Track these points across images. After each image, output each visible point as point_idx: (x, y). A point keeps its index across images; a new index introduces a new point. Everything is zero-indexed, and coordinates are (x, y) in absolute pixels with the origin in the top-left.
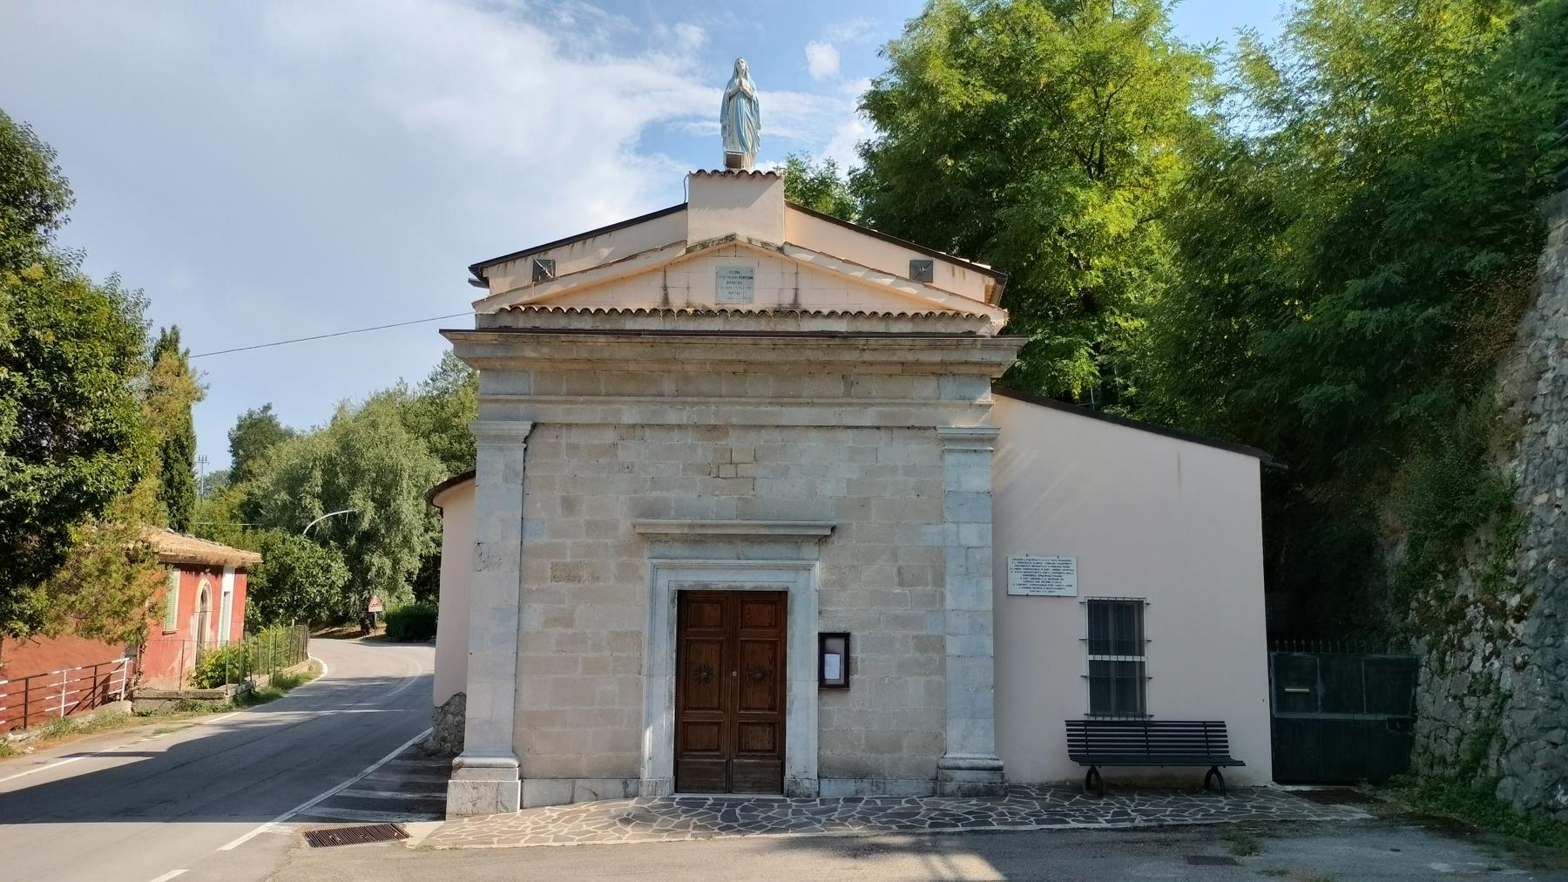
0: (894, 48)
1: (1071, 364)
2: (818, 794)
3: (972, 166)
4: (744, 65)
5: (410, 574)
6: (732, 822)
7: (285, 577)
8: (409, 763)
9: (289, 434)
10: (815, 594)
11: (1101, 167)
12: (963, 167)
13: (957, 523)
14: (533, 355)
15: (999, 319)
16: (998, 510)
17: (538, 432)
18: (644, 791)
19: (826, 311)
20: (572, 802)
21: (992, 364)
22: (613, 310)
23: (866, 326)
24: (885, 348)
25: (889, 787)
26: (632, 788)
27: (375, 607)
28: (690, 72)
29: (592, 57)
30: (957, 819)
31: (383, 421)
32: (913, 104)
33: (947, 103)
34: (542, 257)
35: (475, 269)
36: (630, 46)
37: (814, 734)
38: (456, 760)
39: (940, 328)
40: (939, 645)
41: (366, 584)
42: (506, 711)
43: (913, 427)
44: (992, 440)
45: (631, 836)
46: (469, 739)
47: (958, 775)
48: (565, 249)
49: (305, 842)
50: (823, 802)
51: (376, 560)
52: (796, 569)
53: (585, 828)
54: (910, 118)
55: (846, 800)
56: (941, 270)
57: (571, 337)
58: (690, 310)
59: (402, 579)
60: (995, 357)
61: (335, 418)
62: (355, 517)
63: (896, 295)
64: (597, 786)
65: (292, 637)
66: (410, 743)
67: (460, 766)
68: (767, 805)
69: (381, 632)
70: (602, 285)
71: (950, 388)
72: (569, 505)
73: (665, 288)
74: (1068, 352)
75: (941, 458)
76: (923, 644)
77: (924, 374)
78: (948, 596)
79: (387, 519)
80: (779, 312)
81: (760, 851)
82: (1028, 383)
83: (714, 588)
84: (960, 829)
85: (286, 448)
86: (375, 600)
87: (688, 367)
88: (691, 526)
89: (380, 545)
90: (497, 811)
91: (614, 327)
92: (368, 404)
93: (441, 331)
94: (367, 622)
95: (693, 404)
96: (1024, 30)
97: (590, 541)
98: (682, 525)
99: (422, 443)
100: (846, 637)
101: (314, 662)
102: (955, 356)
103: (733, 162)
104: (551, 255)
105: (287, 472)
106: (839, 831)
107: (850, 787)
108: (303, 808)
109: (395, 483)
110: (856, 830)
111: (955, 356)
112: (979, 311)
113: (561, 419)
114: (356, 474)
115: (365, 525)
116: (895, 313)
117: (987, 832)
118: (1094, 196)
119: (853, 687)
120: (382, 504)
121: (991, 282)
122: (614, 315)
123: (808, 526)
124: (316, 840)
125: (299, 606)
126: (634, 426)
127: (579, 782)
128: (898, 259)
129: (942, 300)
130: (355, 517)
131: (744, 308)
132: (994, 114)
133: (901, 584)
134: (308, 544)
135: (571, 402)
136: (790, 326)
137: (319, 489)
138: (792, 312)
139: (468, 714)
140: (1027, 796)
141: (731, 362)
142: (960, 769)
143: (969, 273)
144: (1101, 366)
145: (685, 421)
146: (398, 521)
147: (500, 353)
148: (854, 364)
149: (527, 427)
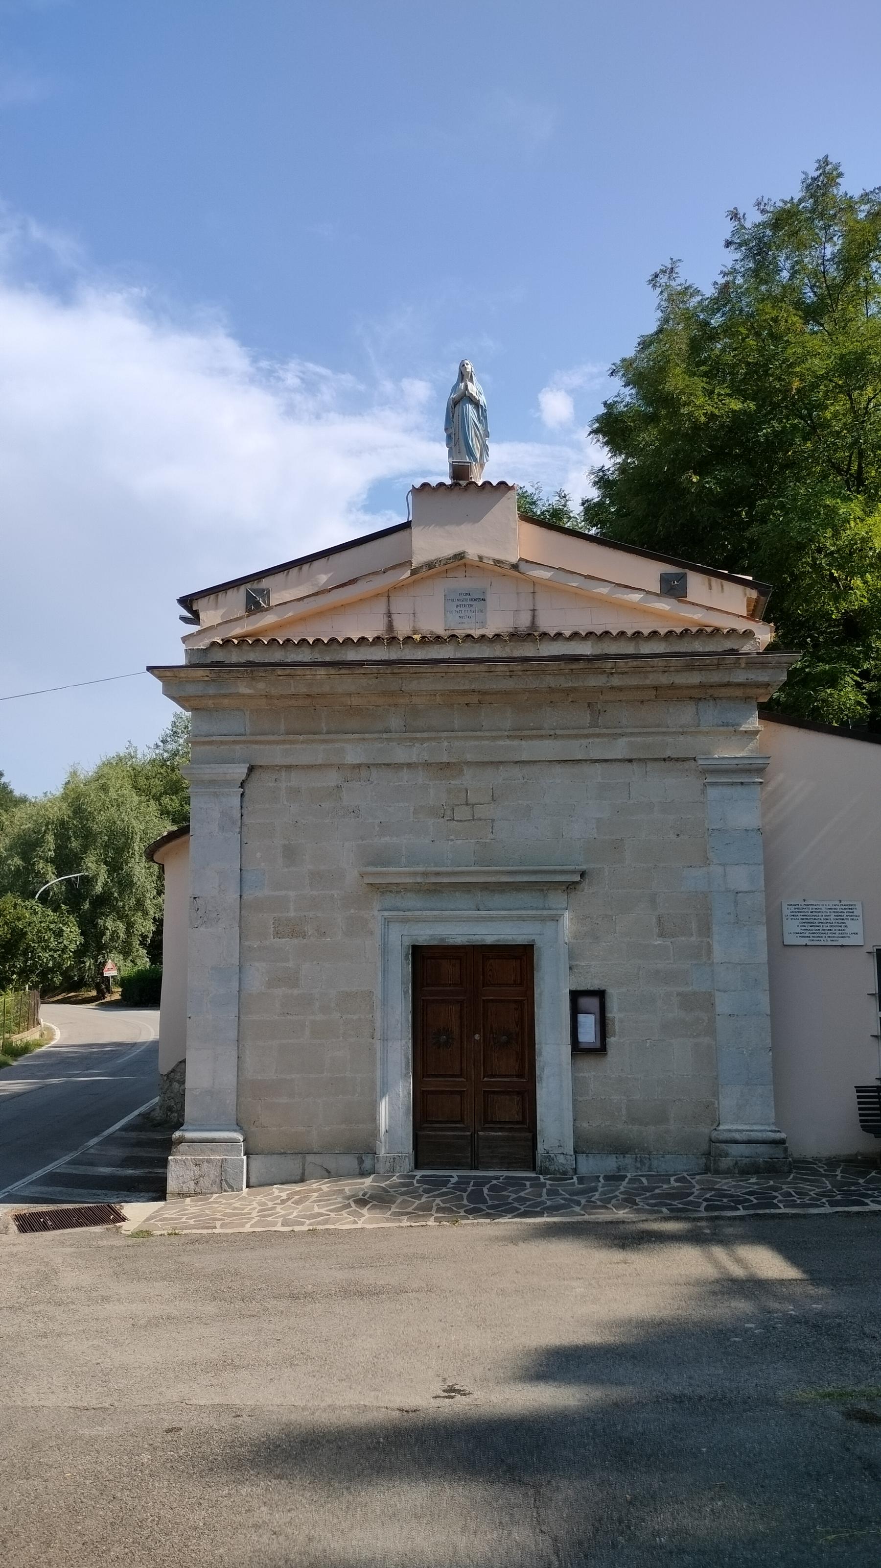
0: (627, 364)
1: (836, 693)
2: (575, 1171)
3: (719, 483)
4: (469, 368)
5: (144, 937)
6: (483, 1204)
7: (17, 942)
8: (133, 1134)
9: (23, 800)
10: (565, 946)
11: (859, 478)
12: (710, 483)
13: (724, 865)
14: (248, 691)
15: (765, 635)
16: (769, 849)
17: (256, 775)
18: (381, 1167)
19: (567, 633)
20: (302, 1180)
21: (758, 685)
22: (333, 640)
23: (613, 648)
24: (636, 670)
25: (655, 1163)
26: (368, 1163)
27: (110, 971)
28: (418, 428)
29: (318, 417)
30: (737, 1202)
31: (114, 784)
32: (653, 419)
33: (690, 415)
34: (256, 585)
35: (187, 602)
36: (356, 405)
37: (568, 1104)
38: (177, 1134)
39: (698, 646)
40: (707, 1002)
41: (101, 948)
42: (229, 1079)
43: (670, 759)
44: (760, 770)
45: (368, 1220)
46: (190, 1111)
47: (734, 1150)
48: (281, 577)
49: (13, 1227)
50: (581, 1180)
51: (109, 924)
52: (543, 919)
53: (316, 1210)
54: (648, 436)
55: (607, 1178)
56: (698, 585)
57: (288, 670)
58: (417, 637)
59: (136, 943)
60: (762, 677)
61: (68, 783)
62: (88, 881)
63: (646, 612)
64: (331, 1162)
65: (20, 1002)
66: (136, 1113)
67: (181, 1140)
68: (519, 1183)
69: (117, 997)
70: (320, 614)
71: (710, 714)
72: (290, 854)
73: (389, 614)
74: (833, 680)
75: (703, 792)
76: (688, 1001)
77: (680, 699)
78: (716, 947)
79: (120, 883)
80: (514, 636)
81: (513, 1240)
82: (795, 708)
83: (451, 942)
84: (741, 1212)
85: (19, 813)
86: (110, 964)
87: (416, 700)
88: (425, 874)
89: (114, 909)
90: (222, 1190)
91: (335, 658)
92: (99, 768)
93: (150, 669)
94: (102, 985)
95: (423, 740)
96: (771, 335)
97: (315, 893)
98: (415, 874)
99: (153, 805)
100: (601, 994)
101: (49, 1029)
102: (715, 677)
103: (460, 473)
104: (265, 583)
105: (19, 837)
106: (603, 1216)
107: (611, 1163)
108: (16, 1186)
109: (127, 846)
110: (622, 1214)
111: (715, 677)
112: (742, 626)
113: (279, 761)
114: (88, 837)
115: (99, 889)
116: (646, 632)
117: (773, 1216)
118: (856, 507)
119: (611, 1051)
120: (114, 867)
121: (754, 594)
122: (335, 646)
123: (554, 872)
124: (26, 1224)
125: (32, 972)
126: (359, 766)
127: (310, 1158)
128: (647, 572)
129: (698, 616)
130: (88, 881)
131: (476, 633)
132: (741, 425)
133: (661, 935)
134: (39, 909)
135: (291, 742)
136: (528, 650)
137: (52, 854)
138: (532, 635)
139: (188, 1085)
140: (815, 1173)
141: (465, 692)
142: (736, 1142)
143: (728, 585)
144: (869, 694)
145: (414, 759)
146: (131, 884)
147: (212, 691)
148: (601, 690)
149: (243, 770)
